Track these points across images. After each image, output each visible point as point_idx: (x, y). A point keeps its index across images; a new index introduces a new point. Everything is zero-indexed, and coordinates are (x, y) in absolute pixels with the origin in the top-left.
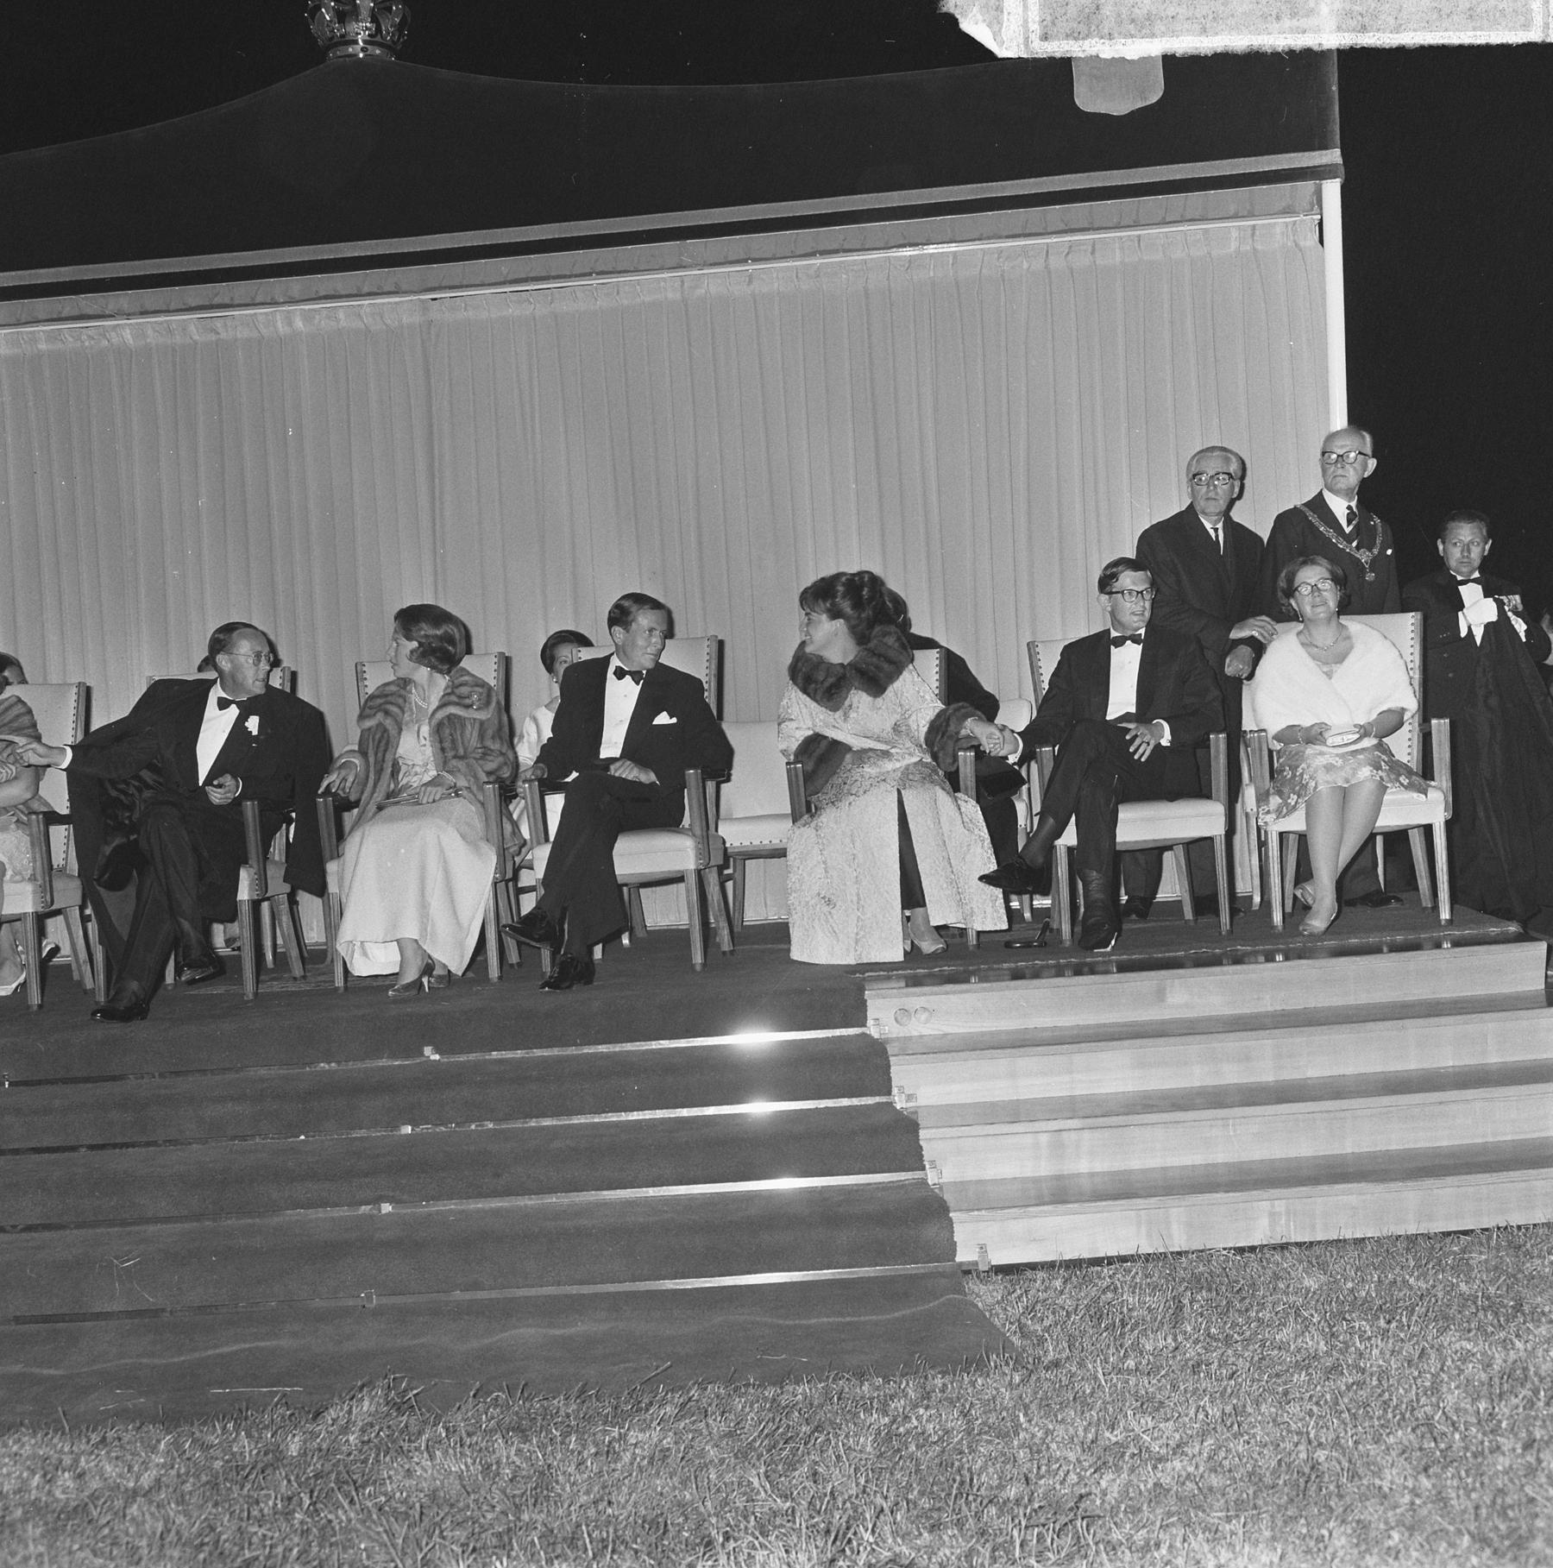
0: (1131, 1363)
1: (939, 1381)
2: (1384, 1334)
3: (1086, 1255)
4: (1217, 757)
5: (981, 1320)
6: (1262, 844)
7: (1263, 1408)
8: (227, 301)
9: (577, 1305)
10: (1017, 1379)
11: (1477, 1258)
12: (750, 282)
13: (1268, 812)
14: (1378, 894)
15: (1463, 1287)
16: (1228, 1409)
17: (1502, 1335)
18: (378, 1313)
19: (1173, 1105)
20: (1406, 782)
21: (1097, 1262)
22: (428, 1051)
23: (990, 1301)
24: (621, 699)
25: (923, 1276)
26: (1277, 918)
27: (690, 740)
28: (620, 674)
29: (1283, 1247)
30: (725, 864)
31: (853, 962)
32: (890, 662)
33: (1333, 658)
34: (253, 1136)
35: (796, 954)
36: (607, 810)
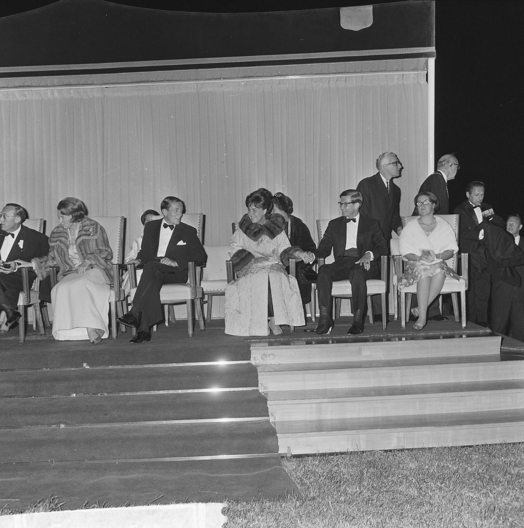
0: (342, 498)
1: (268, 504)
2: (441, 489)
3: (328, 451)
4: (384, 264)
5: (287, 477)
6: (399, 297)
7: (393, 520)
8: (30, 84)
9: (134, 467)
10: (298, 504)
11: (475, 457)
12: (222, 86)
13: (402, 285)
14: (441, 316)
15: (470, 469)
16: (379, 521)
17: (485, 491)
18: (54, 468)
19: (363, 394)
20: (452, 275)
21: (332, 454)
22: (85, 365)
23: (291, 469)
24: (166, 236)
25: (266, 458)
26: (403, 324)
27: (191, 250)
28: (166, 226)
29: (402, 450)
30: (201, 299)
31: (248, 335)
32: (279, 227)
33: (429, 229)
34: (14, 396)
35: (227, 332)
36: (156, 275)
